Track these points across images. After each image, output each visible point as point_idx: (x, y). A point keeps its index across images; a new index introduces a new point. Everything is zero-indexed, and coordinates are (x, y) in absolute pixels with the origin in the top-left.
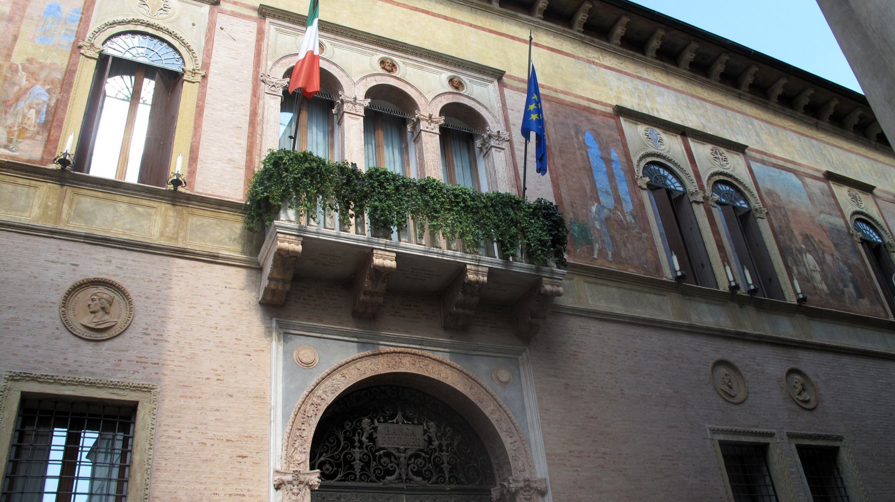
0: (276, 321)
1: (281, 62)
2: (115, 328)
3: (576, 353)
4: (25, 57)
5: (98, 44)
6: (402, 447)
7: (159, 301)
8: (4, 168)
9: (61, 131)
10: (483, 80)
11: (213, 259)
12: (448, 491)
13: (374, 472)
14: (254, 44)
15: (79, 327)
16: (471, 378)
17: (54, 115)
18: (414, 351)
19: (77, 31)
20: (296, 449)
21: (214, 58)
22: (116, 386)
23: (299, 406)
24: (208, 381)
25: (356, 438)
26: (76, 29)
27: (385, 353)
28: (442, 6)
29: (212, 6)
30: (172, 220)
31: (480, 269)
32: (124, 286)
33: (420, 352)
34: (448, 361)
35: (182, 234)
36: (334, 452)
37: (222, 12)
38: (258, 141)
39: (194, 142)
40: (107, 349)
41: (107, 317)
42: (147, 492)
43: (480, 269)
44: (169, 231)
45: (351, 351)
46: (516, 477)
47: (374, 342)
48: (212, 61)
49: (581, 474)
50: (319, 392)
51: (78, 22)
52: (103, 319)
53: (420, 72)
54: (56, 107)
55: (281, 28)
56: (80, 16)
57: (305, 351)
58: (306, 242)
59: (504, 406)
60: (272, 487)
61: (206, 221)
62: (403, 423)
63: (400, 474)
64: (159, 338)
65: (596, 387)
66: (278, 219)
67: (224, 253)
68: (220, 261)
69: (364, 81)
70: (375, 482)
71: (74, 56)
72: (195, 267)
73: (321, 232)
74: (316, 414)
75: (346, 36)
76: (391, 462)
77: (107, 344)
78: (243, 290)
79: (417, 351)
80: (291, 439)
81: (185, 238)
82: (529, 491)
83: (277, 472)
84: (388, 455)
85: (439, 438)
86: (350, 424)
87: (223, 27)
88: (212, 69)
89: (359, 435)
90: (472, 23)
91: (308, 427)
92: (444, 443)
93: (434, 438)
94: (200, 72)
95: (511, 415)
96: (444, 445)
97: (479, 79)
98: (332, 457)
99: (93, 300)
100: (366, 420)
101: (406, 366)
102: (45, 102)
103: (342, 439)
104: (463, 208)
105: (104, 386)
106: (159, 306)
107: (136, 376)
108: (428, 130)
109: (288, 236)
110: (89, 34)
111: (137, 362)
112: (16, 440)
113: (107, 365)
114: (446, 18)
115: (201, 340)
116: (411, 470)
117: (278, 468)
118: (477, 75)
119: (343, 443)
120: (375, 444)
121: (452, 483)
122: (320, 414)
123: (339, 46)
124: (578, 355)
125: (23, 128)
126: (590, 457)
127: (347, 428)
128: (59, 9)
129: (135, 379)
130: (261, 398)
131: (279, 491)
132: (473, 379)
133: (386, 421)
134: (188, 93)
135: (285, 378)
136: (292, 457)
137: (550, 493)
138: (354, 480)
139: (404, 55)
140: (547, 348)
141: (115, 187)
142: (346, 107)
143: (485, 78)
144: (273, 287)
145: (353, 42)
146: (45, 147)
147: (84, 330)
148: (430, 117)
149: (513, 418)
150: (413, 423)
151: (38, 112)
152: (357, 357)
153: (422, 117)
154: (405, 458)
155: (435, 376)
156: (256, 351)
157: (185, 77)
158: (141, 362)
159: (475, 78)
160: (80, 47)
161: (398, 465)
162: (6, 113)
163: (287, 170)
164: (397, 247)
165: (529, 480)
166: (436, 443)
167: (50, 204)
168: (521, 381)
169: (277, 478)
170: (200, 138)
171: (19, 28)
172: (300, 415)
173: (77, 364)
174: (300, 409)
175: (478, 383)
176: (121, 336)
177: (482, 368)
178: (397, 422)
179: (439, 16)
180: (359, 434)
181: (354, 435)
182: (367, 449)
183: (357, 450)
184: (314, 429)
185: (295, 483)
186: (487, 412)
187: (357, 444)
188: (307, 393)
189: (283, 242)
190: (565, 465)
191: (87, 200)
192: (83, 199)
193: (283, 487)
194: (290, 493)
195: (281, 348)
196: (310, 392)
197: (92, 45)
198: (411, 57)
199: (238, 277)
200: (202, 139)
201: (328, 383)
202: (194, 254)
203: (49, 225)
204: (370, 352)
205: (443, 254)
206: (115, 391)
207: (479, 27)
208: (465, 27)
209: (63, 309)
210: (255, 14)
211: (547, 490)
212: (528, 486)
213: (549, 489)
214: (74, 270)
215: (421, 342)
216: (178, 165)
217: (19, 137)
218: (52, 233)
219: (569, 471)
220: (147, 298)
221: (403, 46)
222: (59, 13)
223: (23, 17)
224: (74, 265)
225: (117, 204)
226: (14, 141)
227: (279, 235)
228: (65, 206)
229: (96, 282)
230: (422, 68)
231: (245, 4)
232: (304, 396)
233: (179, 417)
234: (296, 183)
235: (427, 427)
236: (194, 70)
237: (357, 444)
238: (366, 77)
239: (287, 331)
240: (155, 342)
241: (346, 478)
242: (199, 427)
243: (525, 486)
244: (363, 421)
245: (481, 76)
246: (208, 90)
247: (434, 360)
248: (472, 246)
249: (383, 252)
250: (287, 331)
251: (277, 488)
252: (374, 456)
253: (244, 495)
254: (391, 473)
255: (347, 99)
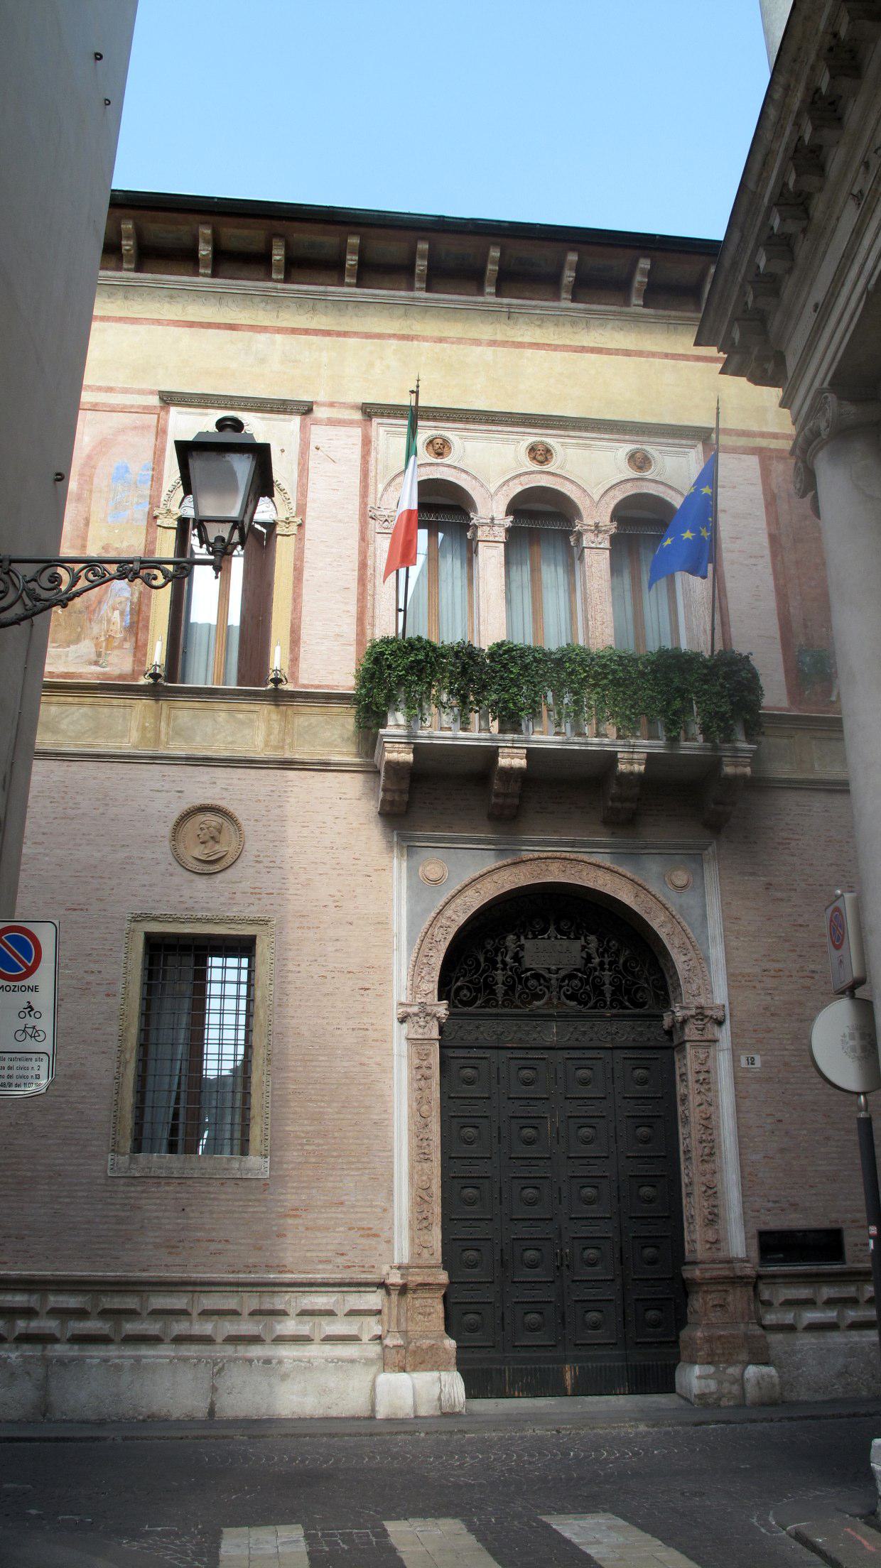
0: (398, 834)
1: (393, 484)
2: (226, 858)
3: (787, 841)
4: (101, 544)
5: (175, 509)
6: (553, 968)
7: (268, 823)
8: (97, 690)
9: (148, 633)
10: (681, 446)
11: (324, 767)
12: (608, 1017)
13: (519, 997)
14: (358, 462)
15: (191, 860)
16: (636, 883)
17: (139, 612)
18: (564, 855)
19: (150, 496)
20: (422, 977)
21: (310, 495)
22: (232, 921)
23: (426, 930)
24: (326, 909)
25: (499, 958)
26: (148, 492)
27: (527, 861)
28: (622, 332)
29: (303, 417)
30: (276, 726)
31: (636, 756)
32: (232, 810)
33: (573, 856)
34: (608, 864)
35: (288, 741)
36: (473, 976)
37: (317, 422)
38: (369, 605)
39: (294, 619)
40: (221, 882)
41: (217, 847)
42: (270, 1028)
43: (636, 756)
44: (274, 739)
45: (489, 861)
46: (687, 1003)
47: (514, 847)
48: (308, 499)
49: (777, 998)
50: (449, 912)
51: (150, 483)
52: (214, 849)
53: (586, 453)
54: (140, 603)
55: (393, 429)
56: (151, 473)
57: (432, 866)
58: (418, 750)
59: (677, 917)
60: (396, 1021)
61: (314, 720)
62: (556, 938)
63: (550, 999)
64: (271, 865)
65: (812, 885)
66: (384, 726)
67: (336, 758)
68: (332, 768)
69: (504, 488)
70: (521, 1008)
71: (150, 530)
72: (306, 778)
73: (433, 735)
74: (445, 938)
75: (480, 422)
76: (540, 985)
77: (219, 876)
78: (359, 799)
79: (567, 855)
80: (417, 968)
81: (291, 745)
82: (702, 1020)
83: (401, 1004)
84: (537, 976)
85: (601, 955)
86: (492, 942)
87: (319, 445)
88: (310, 513)
89: (502, 955)
90: (669, 351)
91: (437, 953)
92: (606, 960)
93: (595, 955)
94: (295, 519)
95: (687, 927)
96: (607, 963)
97: (674, 445)
98: (470, 982)
99: (202, 829)
100: (511, 937)
101: (555, 874)
102: (128, 598)
103: (482, 960)
104: (611, 681)
105: (221, 922)
106: (270, 829)
107: (252, 908)
108: (593, 545)
109: (397, 745)
110: (164, 497)
111: (252, 893)
112: (146, 978)
113: (222, 899)
114: (627, 353)
115: (316, 863)
116: (564, 993)
117: (404, 1000)
118: (670, 441)
119: (483, 965)
120: (520, 964)
121: (615, 1008)
122: (450, 937)
123: (474, 438)
124: (789, 843)
125: (110, 636)
126: (791, 976)
127: (489, 947)
128: (127, 470)
129: (250, 912)
130: (382, 924)
131: (405, 1025)
132: (640, 885)
133: (535, 937)
134: (284, 550)
135: (410, 898)
136: (418, 987)
137: (728, 1022)
138: (495, 1007)
139: (562, 433)
140: (746, 837)
141: (210, 694)
142: (481, 534)
143: (684, 442)
144: (388, 798)
145: (490, 428)
146: (135, 656)
147: (198, 863)
148: (597, 526)
149: (689, 931)
150: (569, 938)
151: (122, 614)
152: (493, 868)
153: (586, 528)
154: (557, 980)
155: (590, 885)
156: (376, 870)
157: (279, 530)
158: (255, 892)
159: (668, 445)
160: (156, 517)
161: (548, 988)
162: (90, 620)
163: (389, 667)
164: (528, 741)
165: (702, 1008)
166: (597, 960)
167: (147, 724)
168: (703, 884)
169: (401, 1011)
170: (301, 612)
171: (89, 507)
172: (427, 940)
173: (193, 900)
174: (426, 933)
175: (645, 889)
176: (234, 866)
177: (652, 870)
178: (549, 938)
179: (617, 352)
180: (502, 953)
181: (496, 955)
182: (511, 971)
183: (499, 972)
184: (442, 955)
185: (421, 1015)
186: (655, 925)
187: (500, 965)
188: (434, 915)
189: (392, 752)
190: (755, 987)
191: (184, 713)
192: (179, 713)
193: (409, 1020)
194: (416, 1026)
195: (405, 864)
196: (438, 913)
197: (169, 511)
198: (572, 433)
199: (353, 785)
200: (304, 613)
201: (459, 901)
202: (303, 763)
203: (149, 752)
204: (509, 861)
205: (587, 744)
206: (232, 926)
207: (679, 355)
208: (657, 361)
209: (174, 843)
210: (358, 416)
211: (724, 1020)
212: (701, 1014)
213: (728, 1017)
214: (179, 797)
215: (572, 844)
216: (278, 659)
217: (107, 649)
218: (154, 759)
219: (759, 994)
220: (256, 820)
221: (559, 421)
222: (127, 475)
223: (91, 492)
224: (179, 792)
225: (215, 714)
226: (103, 654)
227: (386, 745)
228: (163, 724)
229: (203, 808)
230: (590, 446)
231: (344, 403)
232: (431, 919)
233: (298, 949)
234: (401, 681)
235: (586, 942)
236: (287, 519)
237: (500, 965)
238: (508, 481)
239: (412, 844)
240: (268, 870)
241: (486, 1004)
242: (319, 959)
243: (697, 1014)
244: (508, 938)
245: (677, 441)
246: (307, 542)
247: (589, 863)
248: (628, 727)
249: (510, 750)
250: (412, 844)
251: (402, 1020)
252: (520, 979)
253: (367, 1029)
254: (539, 997)
255: (481, 521)
